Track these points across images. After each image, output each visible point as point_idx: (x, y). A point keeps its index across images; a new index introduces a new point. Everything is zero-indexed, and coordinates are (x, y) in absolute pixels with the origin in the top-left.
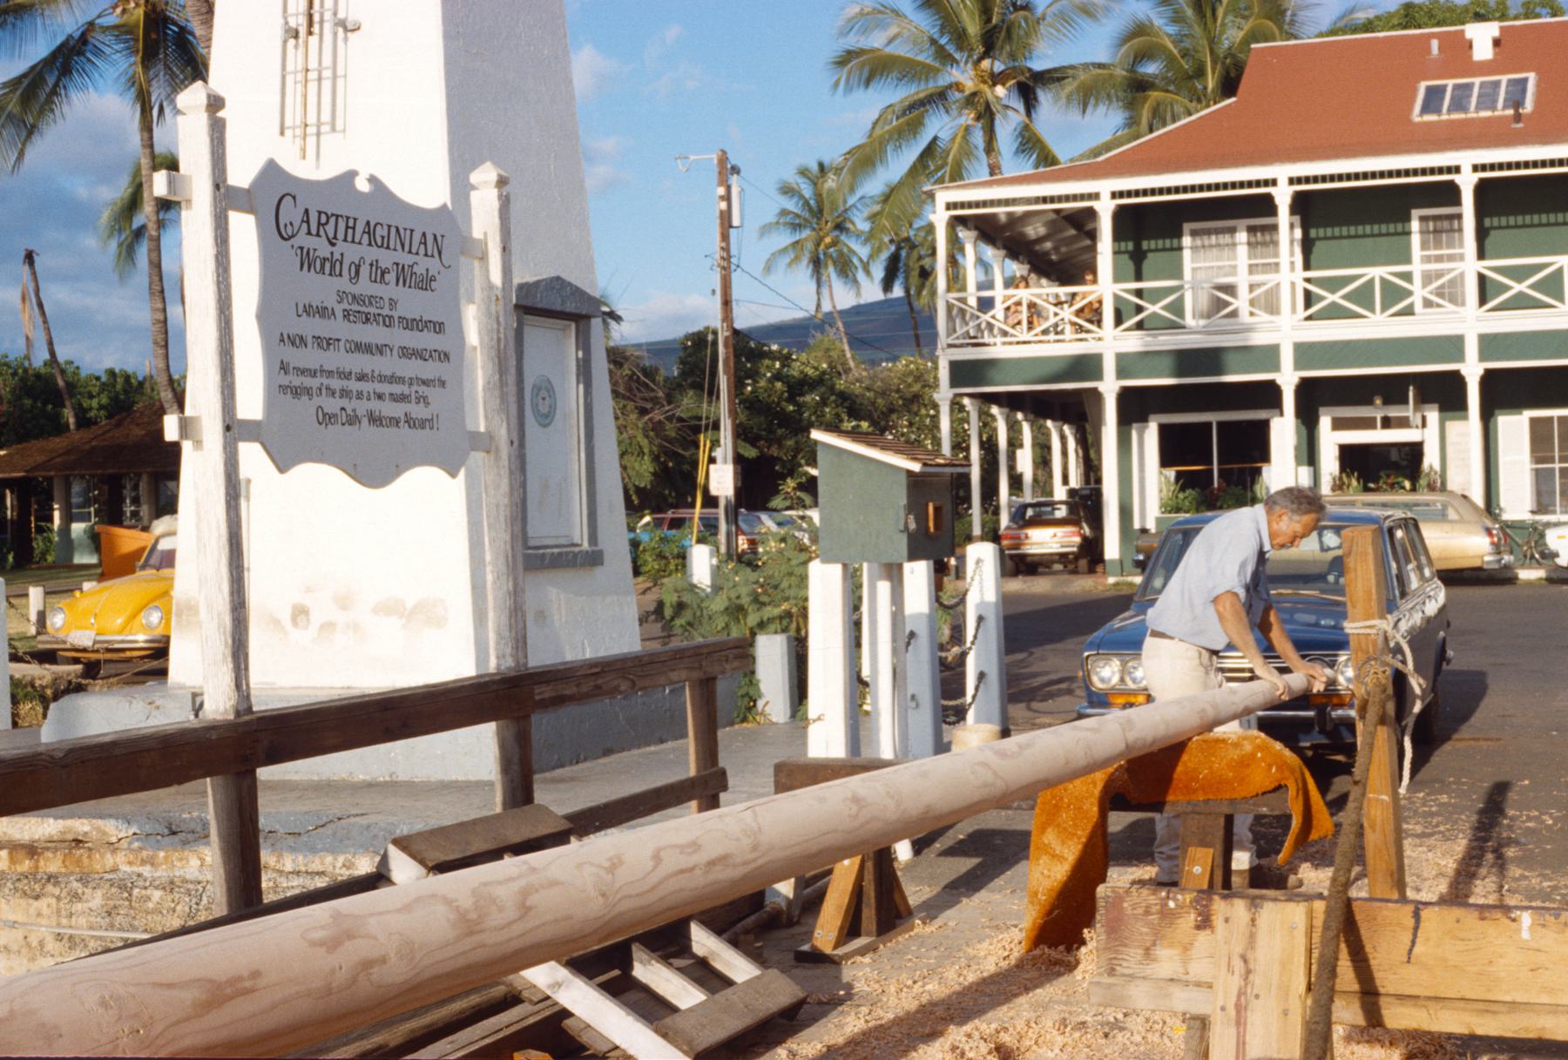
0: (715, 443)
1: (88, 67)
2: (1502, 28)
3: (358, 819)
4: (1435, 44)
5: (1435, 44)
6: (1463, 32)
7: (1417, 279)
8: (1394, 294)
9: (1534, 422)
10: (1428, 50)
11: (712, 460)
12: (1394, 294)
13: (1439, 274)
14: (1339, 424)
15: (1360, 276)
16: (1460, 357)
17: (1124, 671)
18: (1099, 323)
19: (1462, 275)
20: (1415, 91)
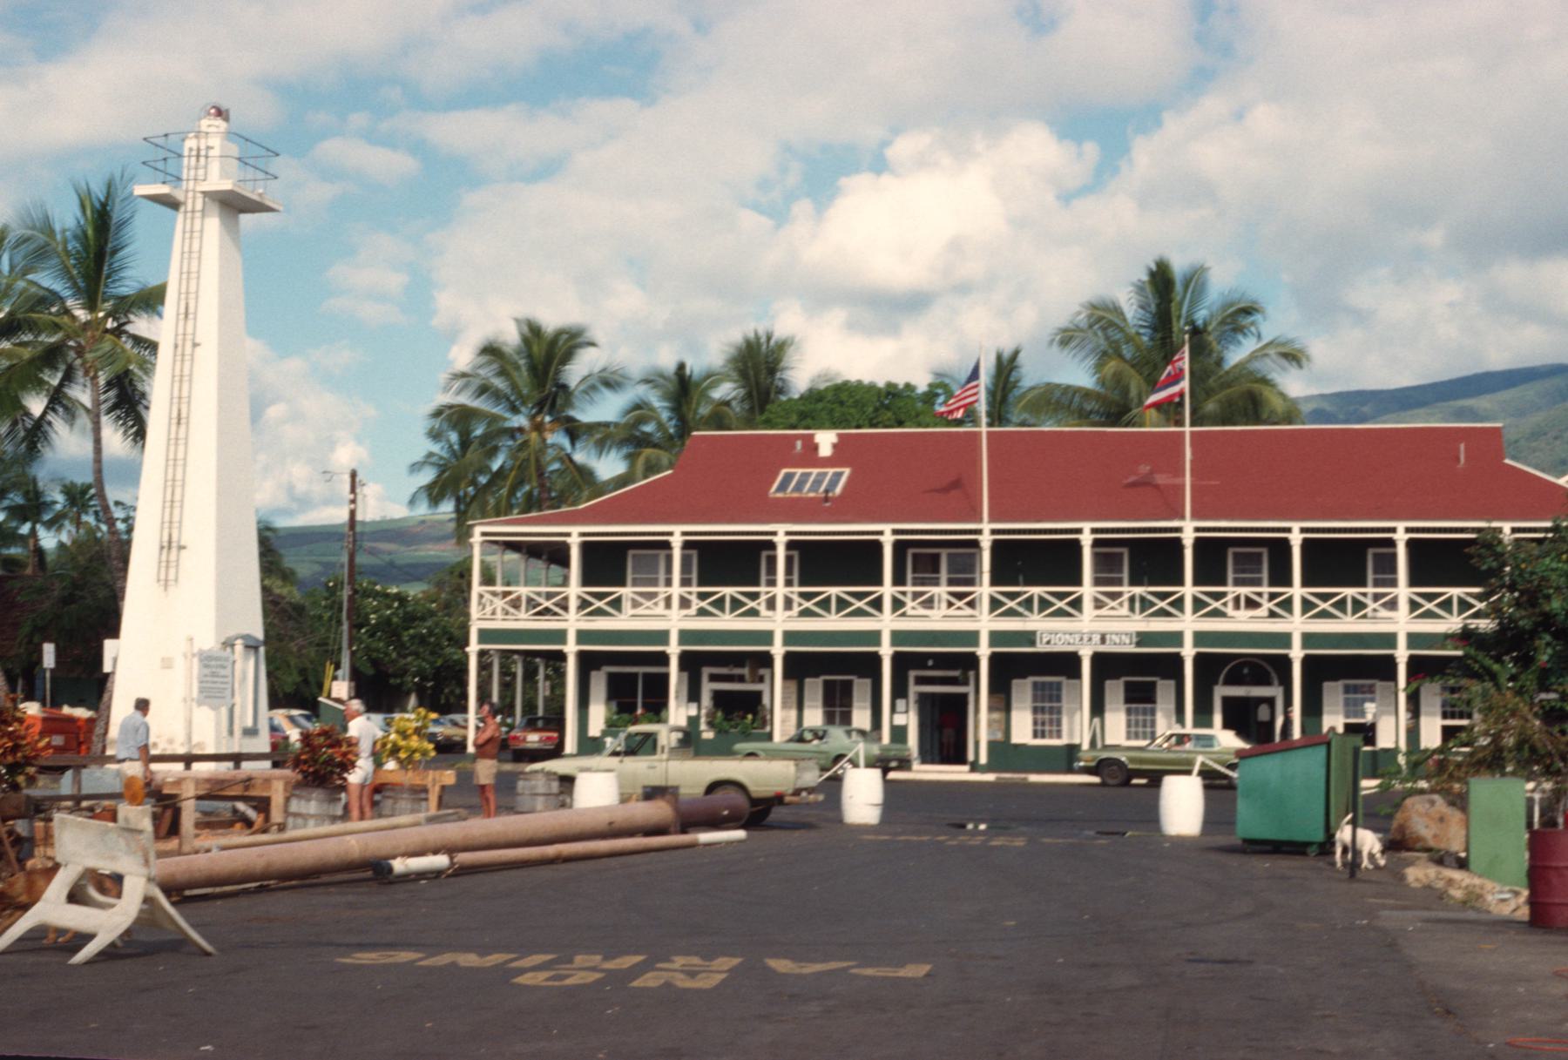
0: (338, 667)
1: (1080, 356)
2: (839, 436)
3: (1395, 913)
4: (799, 444)
5: (799, 444)
6: (812, 436)
7: (1266, 596)
8: (1358, 605)
9: (826, 683)
10: (794, 447)
11: (335, 678)
12: (1358, 605)
13: (922, 594)
14: (713, 678)
15: (558, 594)
16: (1181, 644)
17: (77, 781)
18: (1181, 610)
19: (1396, 598)
20: (777, 474)
